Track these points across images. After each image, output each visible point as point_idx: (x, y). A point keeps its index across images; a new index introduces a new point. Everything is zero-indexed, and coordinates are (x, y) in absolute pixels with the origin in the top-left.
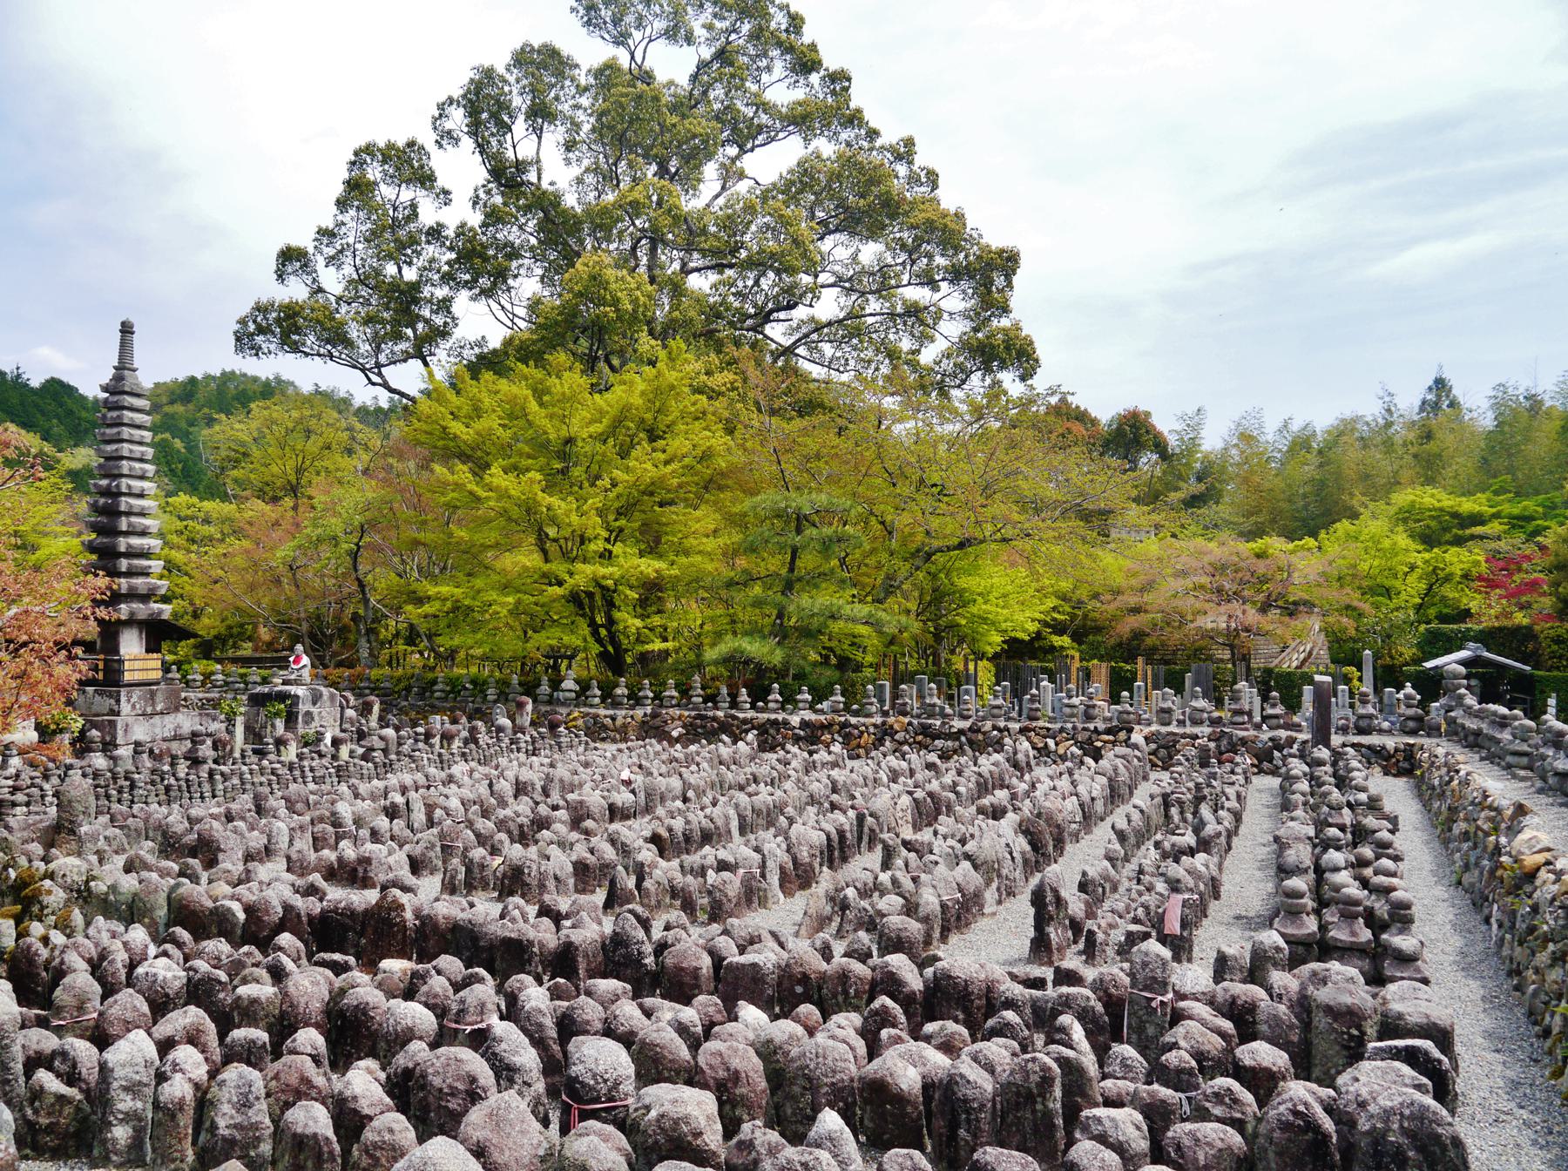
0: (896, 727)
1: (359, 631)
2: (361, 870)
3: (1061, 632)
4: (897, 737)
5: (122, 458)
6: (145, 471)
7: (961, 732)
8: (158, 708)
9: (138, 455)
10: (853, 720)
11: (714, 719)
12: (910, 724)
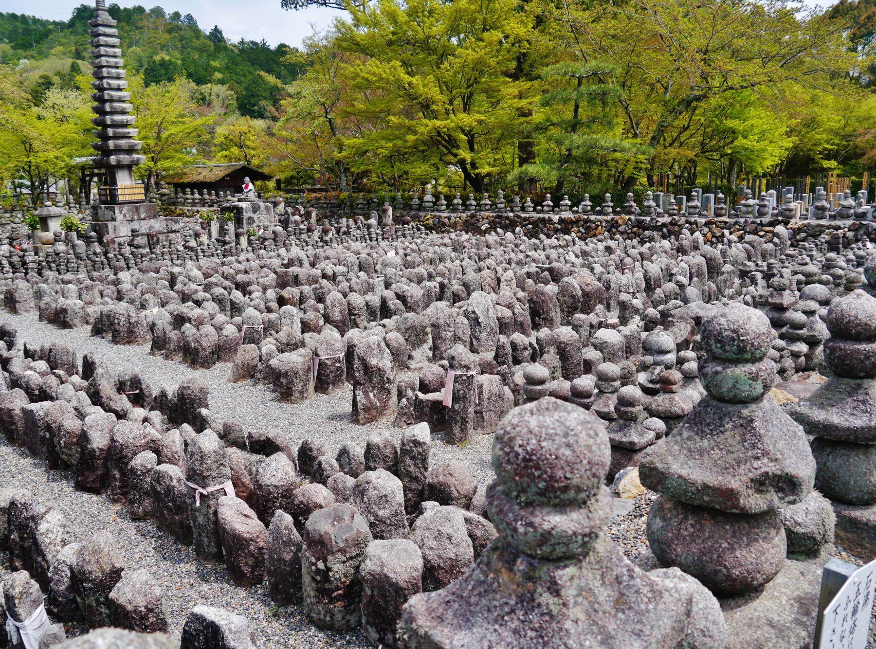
0: (620, 222)
1: (339, 170)
2: (62, 316)
3: (828, 158)
4: (620, 229)
5: (103, 67)
6: (119, 74)
7: (664, 225)
8: (142, 216)
9: (113, 64)
10: (593, 217)
11: (507, 218)
12: (629, 220)
